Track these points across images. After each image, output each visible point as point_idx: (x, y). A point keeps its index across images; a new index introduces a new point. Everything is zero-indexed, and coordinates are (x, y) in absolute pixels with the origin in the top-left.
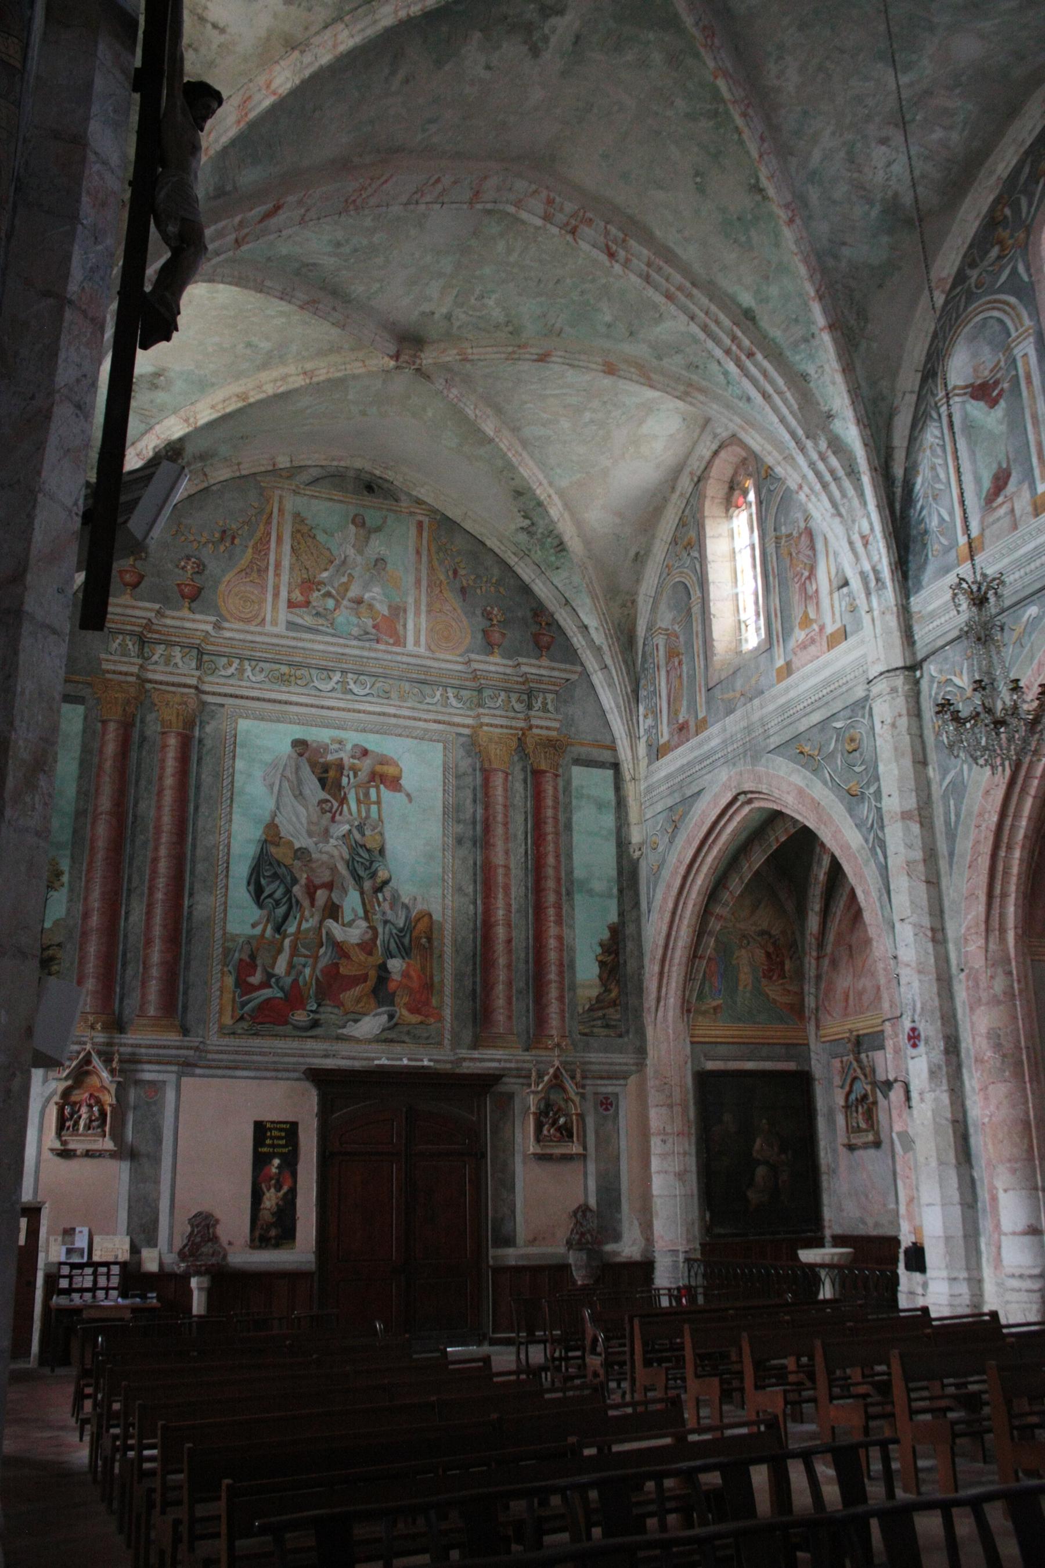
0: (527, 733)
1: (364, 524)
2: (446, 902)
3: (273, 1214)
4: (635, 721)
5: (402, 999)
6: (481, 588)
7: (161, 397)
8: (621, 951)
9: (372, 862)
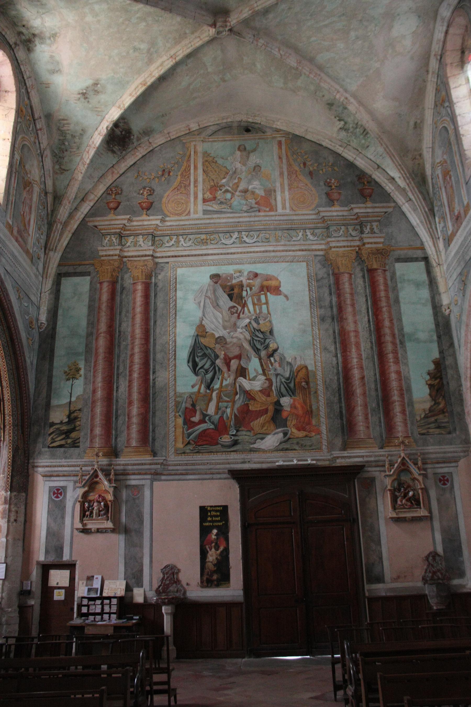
0: (362, 248)
1: (245, 149)
2: (317, 357)
3: (215, 565)
4: (434, 228)
5: (292, 422)
6: (322, 170)
7: (102, 97)
8: (444, 376)
9: (265, 340)
